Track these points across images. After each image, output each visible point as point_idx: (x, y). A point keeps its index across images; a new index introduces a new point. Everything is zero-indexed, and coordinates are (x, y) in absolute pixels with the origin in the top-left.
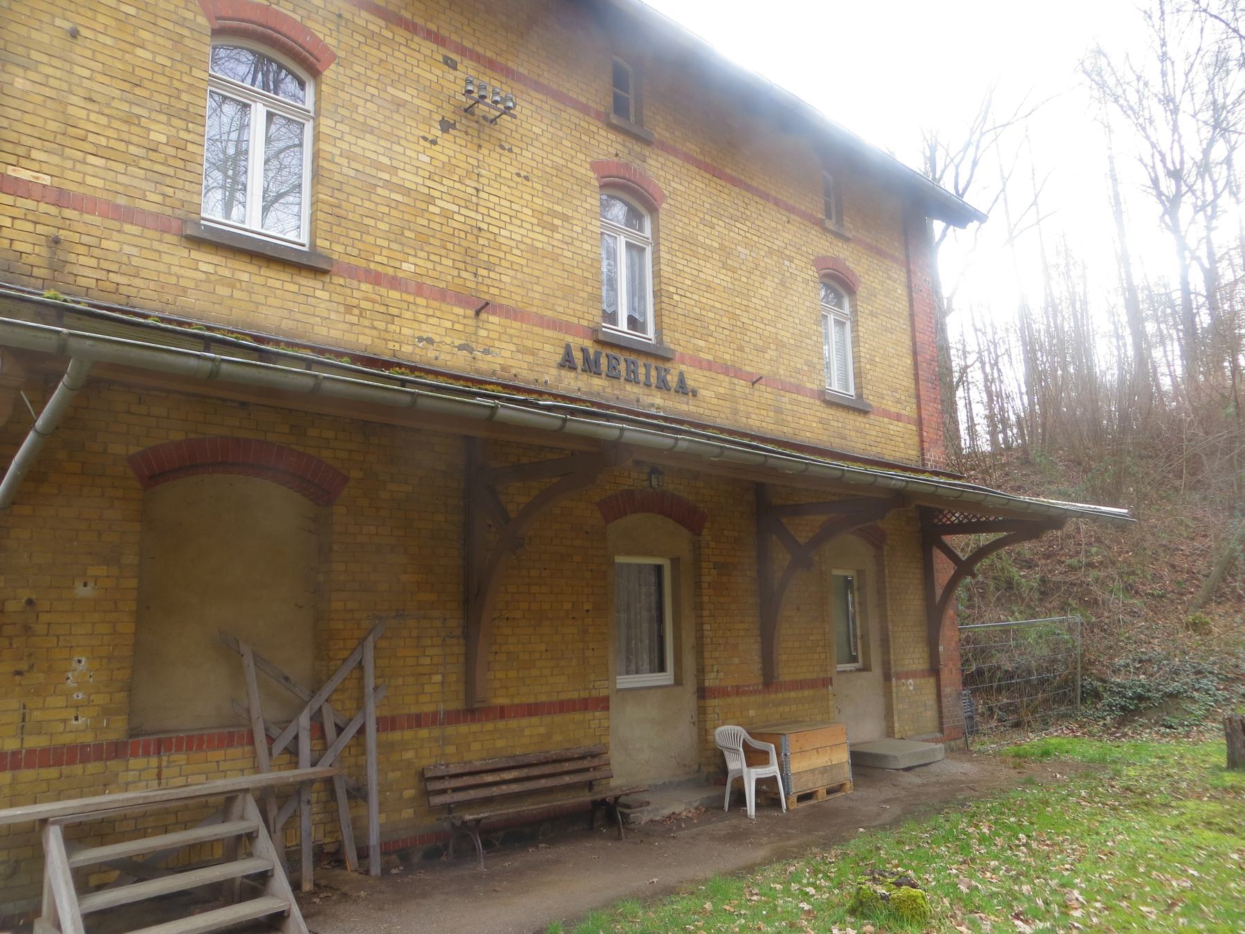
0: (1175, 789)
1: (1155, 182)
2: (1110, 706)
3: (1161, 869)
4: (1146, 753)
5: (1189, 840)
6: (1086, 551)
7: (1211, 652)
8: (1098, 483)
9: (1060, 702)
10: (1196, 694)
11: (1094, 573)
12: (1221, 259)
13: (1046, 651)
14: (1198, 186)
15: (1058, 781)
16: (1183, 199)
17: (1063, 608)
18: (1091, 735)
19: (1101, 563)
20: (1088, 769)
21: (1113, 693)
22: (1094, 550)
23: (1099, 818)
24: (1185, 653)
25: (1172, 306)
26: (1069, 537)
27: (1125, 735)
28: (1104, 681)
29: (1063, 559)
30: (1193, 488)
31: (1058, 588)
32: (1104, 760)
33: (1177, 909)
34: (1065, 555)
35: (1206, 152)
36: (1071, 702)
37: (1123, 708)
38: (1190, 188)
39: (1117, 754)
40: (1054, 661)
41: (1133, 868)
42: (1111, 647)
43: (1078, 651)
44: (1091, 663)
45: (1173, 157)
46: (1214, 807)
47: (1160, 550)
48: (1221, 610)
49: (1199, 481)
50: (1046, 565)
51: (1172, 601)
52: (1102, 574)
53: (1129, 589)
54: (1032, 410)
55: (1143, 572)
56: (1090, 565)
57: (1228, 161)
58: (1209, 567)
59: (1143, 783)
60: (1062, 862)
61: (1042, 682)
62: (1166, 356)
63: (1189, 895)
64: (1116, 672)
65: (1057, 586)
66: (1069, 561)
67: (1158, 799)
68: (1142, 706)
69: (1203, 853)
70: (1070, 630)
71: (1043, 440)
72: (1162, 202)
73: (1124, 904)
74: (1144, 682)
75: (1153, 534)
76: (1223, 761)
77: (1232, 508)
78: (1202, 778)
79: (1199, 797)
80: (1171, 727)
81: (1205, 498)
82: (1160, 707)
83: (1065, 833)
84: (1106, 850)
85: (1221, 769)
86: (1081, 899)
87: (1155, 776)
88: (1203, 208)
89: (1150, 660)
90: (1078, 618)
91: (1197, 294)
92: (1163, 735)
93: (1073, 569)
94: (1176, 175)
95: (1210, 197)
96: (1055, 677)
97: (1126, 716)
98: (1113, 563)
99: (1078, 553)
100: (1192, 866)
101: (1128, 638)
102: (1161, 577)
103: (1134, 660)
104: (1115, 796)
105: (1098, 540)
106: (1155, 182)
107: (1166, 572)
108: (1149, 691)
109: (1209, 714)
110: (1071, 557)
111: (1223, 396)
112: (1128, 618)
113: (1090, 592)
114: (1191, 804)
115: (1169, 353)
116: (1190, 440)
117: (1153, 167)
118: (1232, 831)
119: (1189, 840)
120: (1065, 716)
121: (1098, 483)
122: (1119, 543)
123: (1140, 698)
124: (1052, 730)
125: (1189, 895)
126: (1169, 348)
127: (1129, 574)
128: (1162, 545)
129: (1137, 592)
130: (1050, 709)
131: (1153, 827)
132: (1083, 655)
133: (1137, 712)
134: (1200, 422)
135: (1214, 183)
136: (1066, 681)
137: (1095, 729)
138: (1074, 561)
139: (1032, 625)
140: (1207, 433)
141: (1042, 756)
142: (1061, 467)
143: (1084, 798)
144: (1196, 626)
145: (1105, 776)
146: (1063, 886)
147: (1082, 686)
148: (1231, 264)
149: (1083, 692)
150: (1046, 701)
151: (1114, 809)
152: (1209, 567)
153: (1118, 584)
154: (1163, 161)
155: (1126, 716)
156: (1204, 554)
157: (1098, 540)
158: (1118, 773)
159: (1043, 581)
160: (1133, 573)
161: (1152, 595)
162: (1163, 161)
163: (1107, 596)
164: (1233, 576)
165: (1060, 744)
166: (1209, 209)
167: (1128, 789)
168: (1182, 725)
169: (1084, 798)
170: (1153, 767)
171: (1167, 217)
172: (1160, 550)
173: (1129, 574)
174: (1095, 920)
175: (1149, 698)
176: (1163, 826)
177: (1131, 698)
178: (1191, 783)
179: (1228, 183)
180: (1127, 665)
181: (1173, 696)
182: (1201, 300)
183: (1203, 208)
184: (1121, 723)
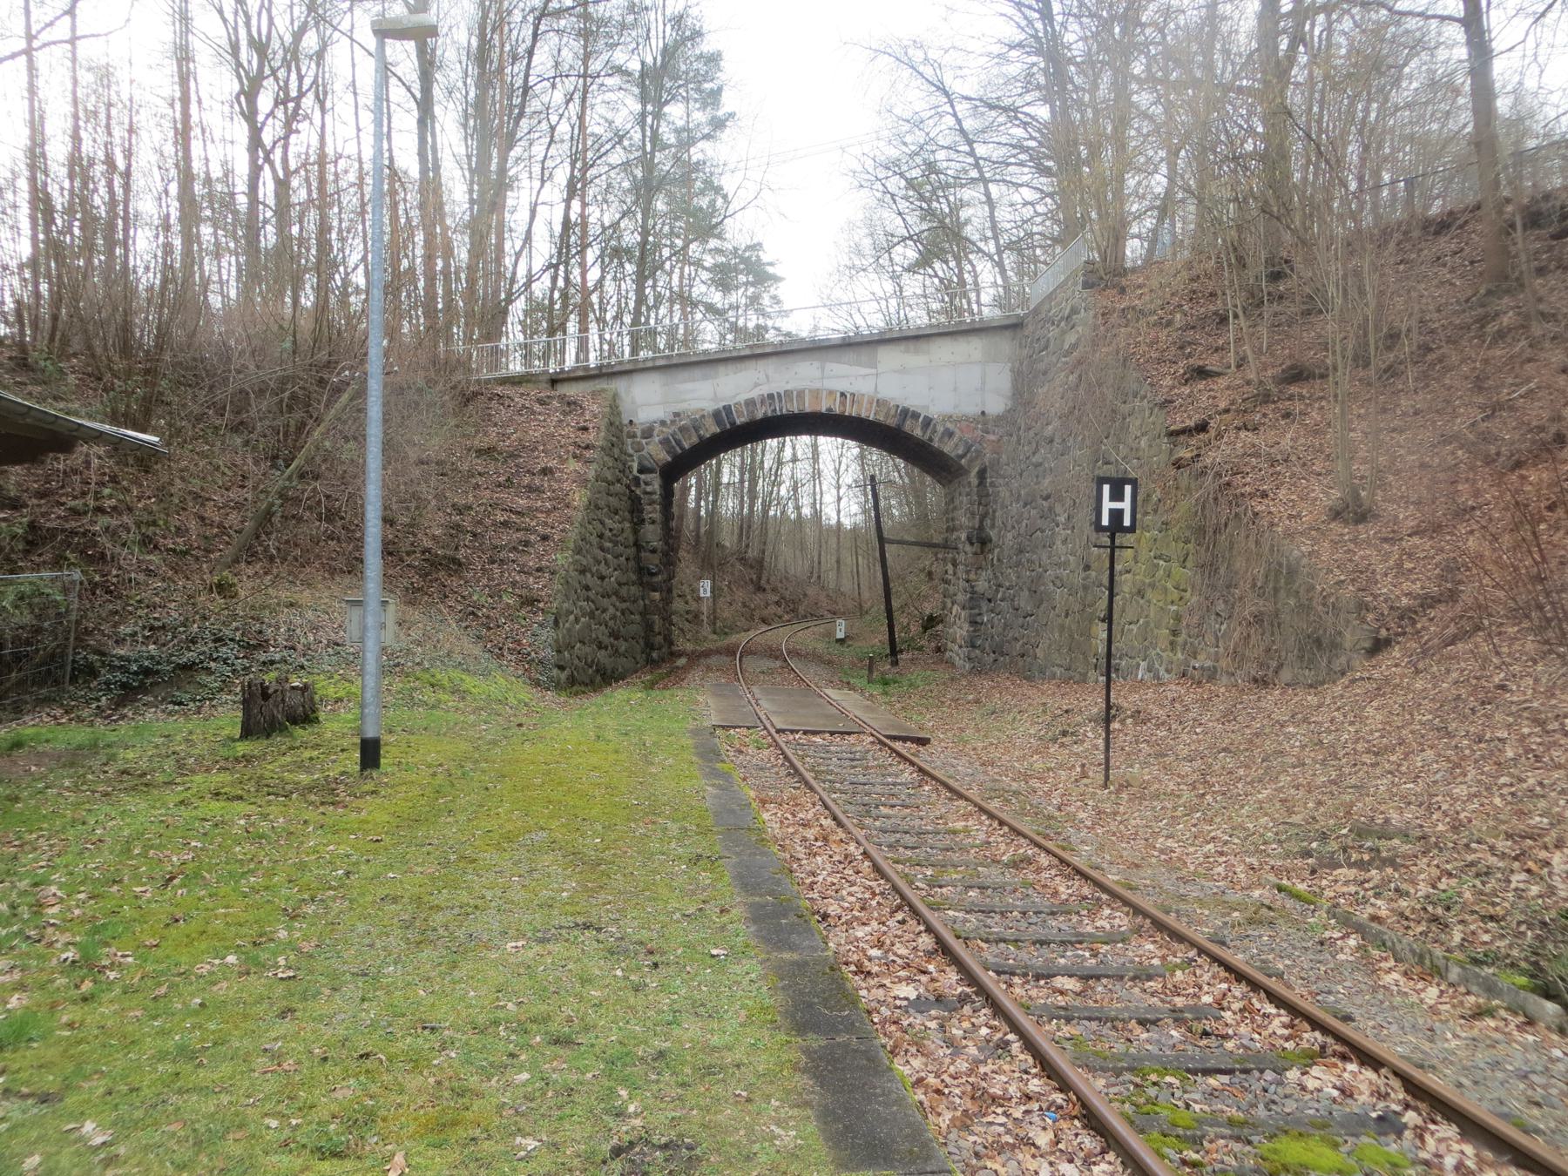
0: (180, 765)
1: (235, 49)
2: (108, 683)
3: (160, 847)
4: (147, 733)
5: (194, 813)
6: (96, 493)
7: (235, 617)
8: (122, 408)
9: (42, 684)
10: (212, 664)
11: (104, 520)
12: (297, 171)
13: (27, 618)
14: (282, 74)
15: (32, 774)
16: (265, 83)
17: (58, 562)
18: (80, 720)
19: (114, 508)
20: (73, 758)
21: (113, 668)
22: (107, 491)
23: (87, 806)
24: (205, 618)
25: (235, 213)
26: (75, 472)
27: (123, 717)
28: (103, 654)
29: (64, 499)
30: (235, 429)
31: (54, 536)
32: (96, 745)
33: (176, 882)
34: (67, 495)
35: (298, 36)
36: (56, 682)
37: (124, 686)
38: (274, 72)
39: (112, 737)
40: (38, 630)
41: (127, 851)
42: (116, 612)
43: (73, 617)
44: (88, 632)
45: (260, 25)
46: (226, 777)
47: (189, 498)
48: (250, 572)
49: (242, 423)
50: (39, 506)
51: (197, 559)
52: (115, 522)
53: (147, 543)
54: (37, 294)
55: (166, 522)
56: (100, 510)
57: (320, 56)
58: (242, 522)
59: (144, 764)
60: (35, 860)
61: (17, 658)
62: (219, 272)
63: (191, 865)
64: (120, 642)
65: (53, 533)
66: (72, 503)
67: (160, 778)
68: (148, 681)
69: (207, 825)
70: (65, 590)
71: (52, 339)
72: (239, 77)
73: (116, 888)
74: (153, 653)
75: (183, 479)
76: (237, 732)
77: (275, 457)
78: (213, 752)
79: (208, 771)
80: (180, 704)
81: (247, 443)
82: (170, 682)
83: (41, 829)
84: (94, 839)
85: (234, 741)
86: (59, 893)
87: (159, 755)
88: (284, 103)
89: (163, 627)
90: (77, 575)
91: (266, 206)
92: (170, 714)
93: (75, 512)
94: (261, 48)
95: (294, 94)
96: (37, 650)
97: (126, 695)
98: (130, 509)
99: (84, 494)
100: (194, 838)
101: (140, 602)
102: (187, 530)
103: (144, 627)
104: (108, 782)
105: (114, 479)
106: (235, 49)
107: (193, 525)
108: (159, 663)
109: (226, 686)
110: (75, 498)
111: (281, 327)
112: (141, 577)
113: (95, 544)
114: (198, 778)
115: (224, 272)
116: (239, 372)
117: (236, 29)
118: (240, 798)
119: (194, 813)
120: (47, 701)
121: (122, 408)
122: (141, 486)
123: (147, 672)
124: (26, 718)
125: (191, 865)
126: (224, 264)
127: (148, 524)
128: (190, 492)
129: (156, 547)
130: (27, 692)
131: (153, 807)
132: (78, 622)
133: (143, 689)
134: (253, 352)
135: (301, 78)
136: (53, 656)
137: (85, 713)
138: (78, 503)
139: (11, 583)
140: (258, 367)
141: (11, 749)
142: (72, 379)
143: (68, 789)
144: (222, 588)
145: (96, 763)
146: (36, 885)
147: (74, 661)
148: (307, 180)
149: (73, 669)
150: (20, 683)
151: (106, 794)
152: (242, 522)
153: (135, 535)
154: (248, 24)
155: (126, 695)
156: (239, 506)
157: (114, 479)
158: (112, 758)
159: (32, 526)
160: (154, 523)
161: (174, 551)
162: (248, 24)
163: (118, 550)
164: (267, 534)
165: (38, 734)
166: (291, 105)
167: (124, 772)
168: (194, 700)
169: (68, 789)
170: (157, 747)
171: (242, 99)
172: (189, 498)
173: (148, 524)
174: (77, 912)
175: (158, 672)
176: (164, 805)
177: (136, 673)
178: (199, 759)
179: (315, 82)
180: (135, 633)
181: (189, 667)
182: (269, 214)
183: (284, 103)
184: (120, 703)
